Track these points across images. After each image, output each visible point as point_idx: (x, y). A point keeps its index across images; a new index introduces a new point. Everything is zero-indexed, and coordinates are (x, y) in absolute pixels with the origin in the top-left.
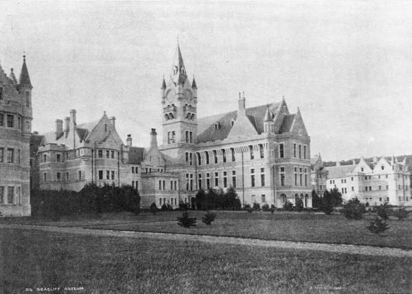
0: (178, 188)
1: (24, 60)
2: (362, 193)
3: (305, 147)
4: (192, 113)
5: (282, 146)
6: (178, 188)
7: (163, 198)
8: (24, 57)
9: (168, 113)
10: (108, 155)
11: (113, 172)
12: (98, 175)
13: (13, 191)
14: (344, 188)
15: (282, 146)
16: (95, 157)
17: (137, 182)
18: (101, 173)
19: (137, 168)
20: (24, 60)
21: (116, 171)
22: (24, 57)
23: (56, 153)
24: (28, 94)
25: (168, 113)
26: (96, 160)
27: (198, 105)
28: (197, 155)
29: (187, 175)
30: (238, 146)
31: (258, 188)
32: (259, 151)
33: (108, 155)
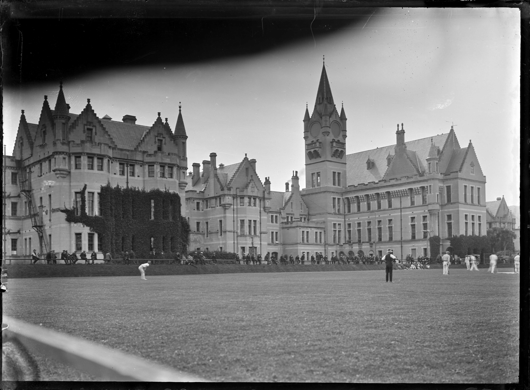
0: (323, 241)
1: (180, 111)
2: (281, 224)
3: (479, 189)
4: (340, 150)
5: (448, 188)
6: (323, 241)
7: (306, 252)
8: (180, 107)
9: (312, 150)
10: (250, 203)
11: (255, 221)
12: (239, 225)
13: (76, 165)
14: (252, 220)
15: (448, 188)
16: (237, 206)
17: (276, 233)
18: (242, 221)
19: (276, 216)
20: (180, 111)
21: (258, 220)
22: (180, 107)
23: (196, 201)
24: (184, 144)
25: (312, 150)
26: (237, 208)
27: (348, 141)
28: (346, 201)
29: (335, 224)
30: (361, 194)
31: (419, 240)
32: (421, 196)
33: (250, 203)
